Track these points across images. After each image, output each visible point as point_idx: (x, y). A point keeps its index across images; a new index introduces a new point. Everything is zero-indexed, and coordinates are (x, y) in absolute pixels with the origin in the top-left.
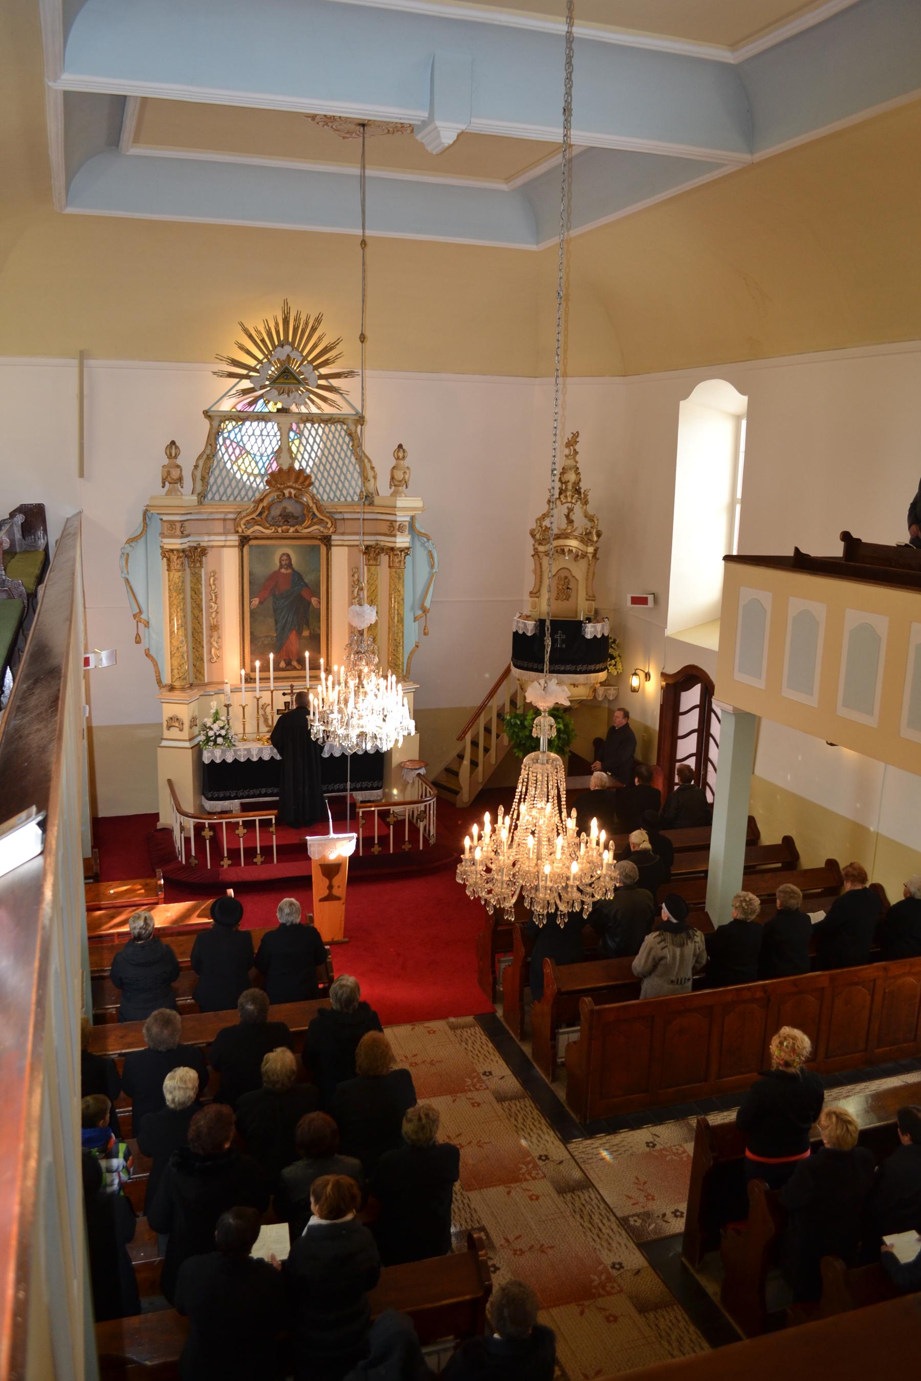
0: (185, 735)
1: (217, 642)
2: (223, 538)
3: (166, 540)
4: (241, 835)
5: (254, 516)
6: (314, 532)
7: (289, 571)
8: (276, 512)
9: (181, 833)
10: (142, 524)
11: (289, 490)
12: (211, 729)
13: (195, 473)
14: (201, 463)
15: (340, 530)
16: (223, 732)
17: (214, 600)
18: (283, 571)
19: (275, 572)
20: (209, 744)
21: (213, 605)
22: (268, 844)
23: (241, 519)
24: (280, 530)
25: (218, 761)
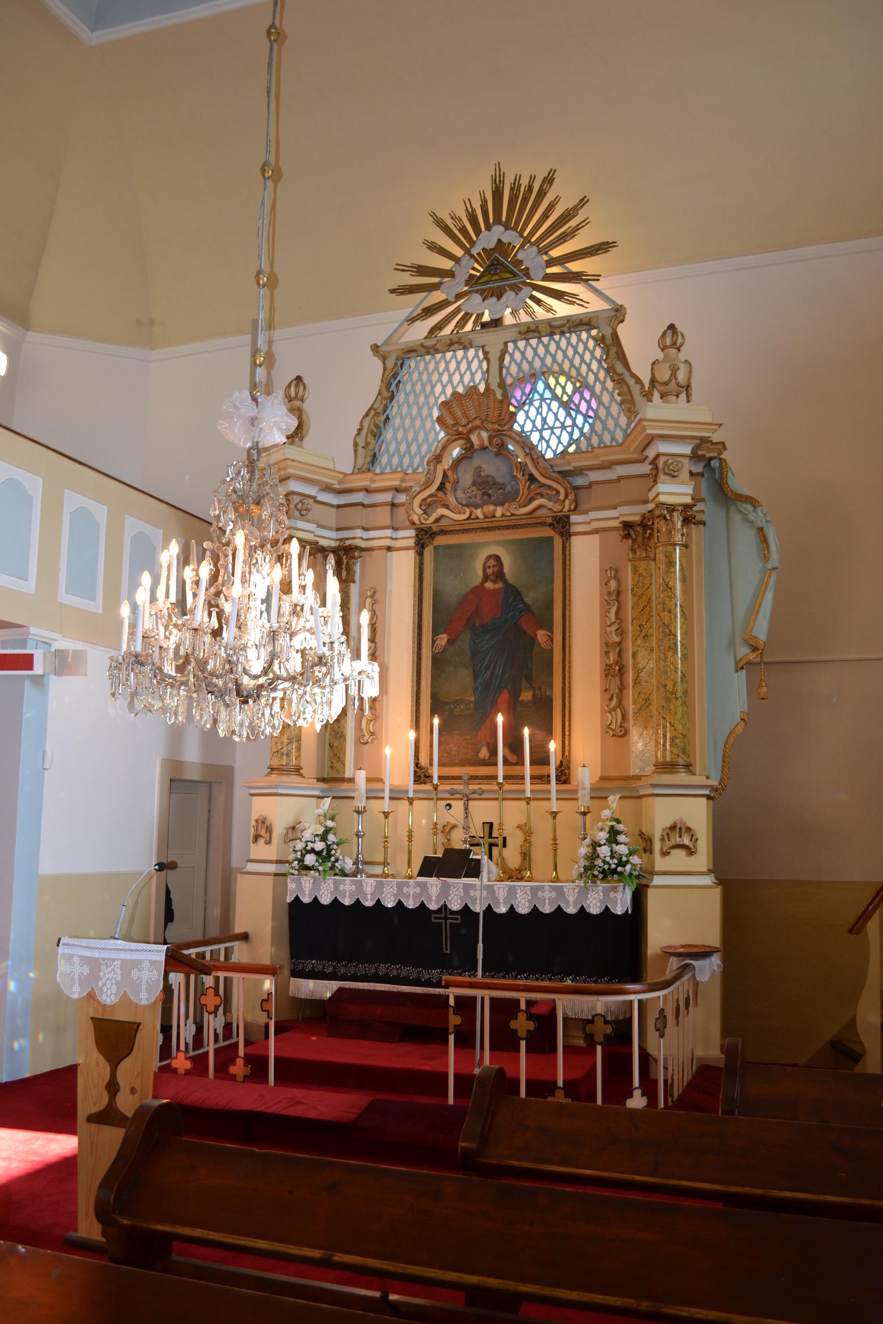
2: (388, 533)
7: (499, 585)
13: (358, 440)
18: (489, 585)
19: (476, 588)
24: (479, 513)
25: (306, 900)
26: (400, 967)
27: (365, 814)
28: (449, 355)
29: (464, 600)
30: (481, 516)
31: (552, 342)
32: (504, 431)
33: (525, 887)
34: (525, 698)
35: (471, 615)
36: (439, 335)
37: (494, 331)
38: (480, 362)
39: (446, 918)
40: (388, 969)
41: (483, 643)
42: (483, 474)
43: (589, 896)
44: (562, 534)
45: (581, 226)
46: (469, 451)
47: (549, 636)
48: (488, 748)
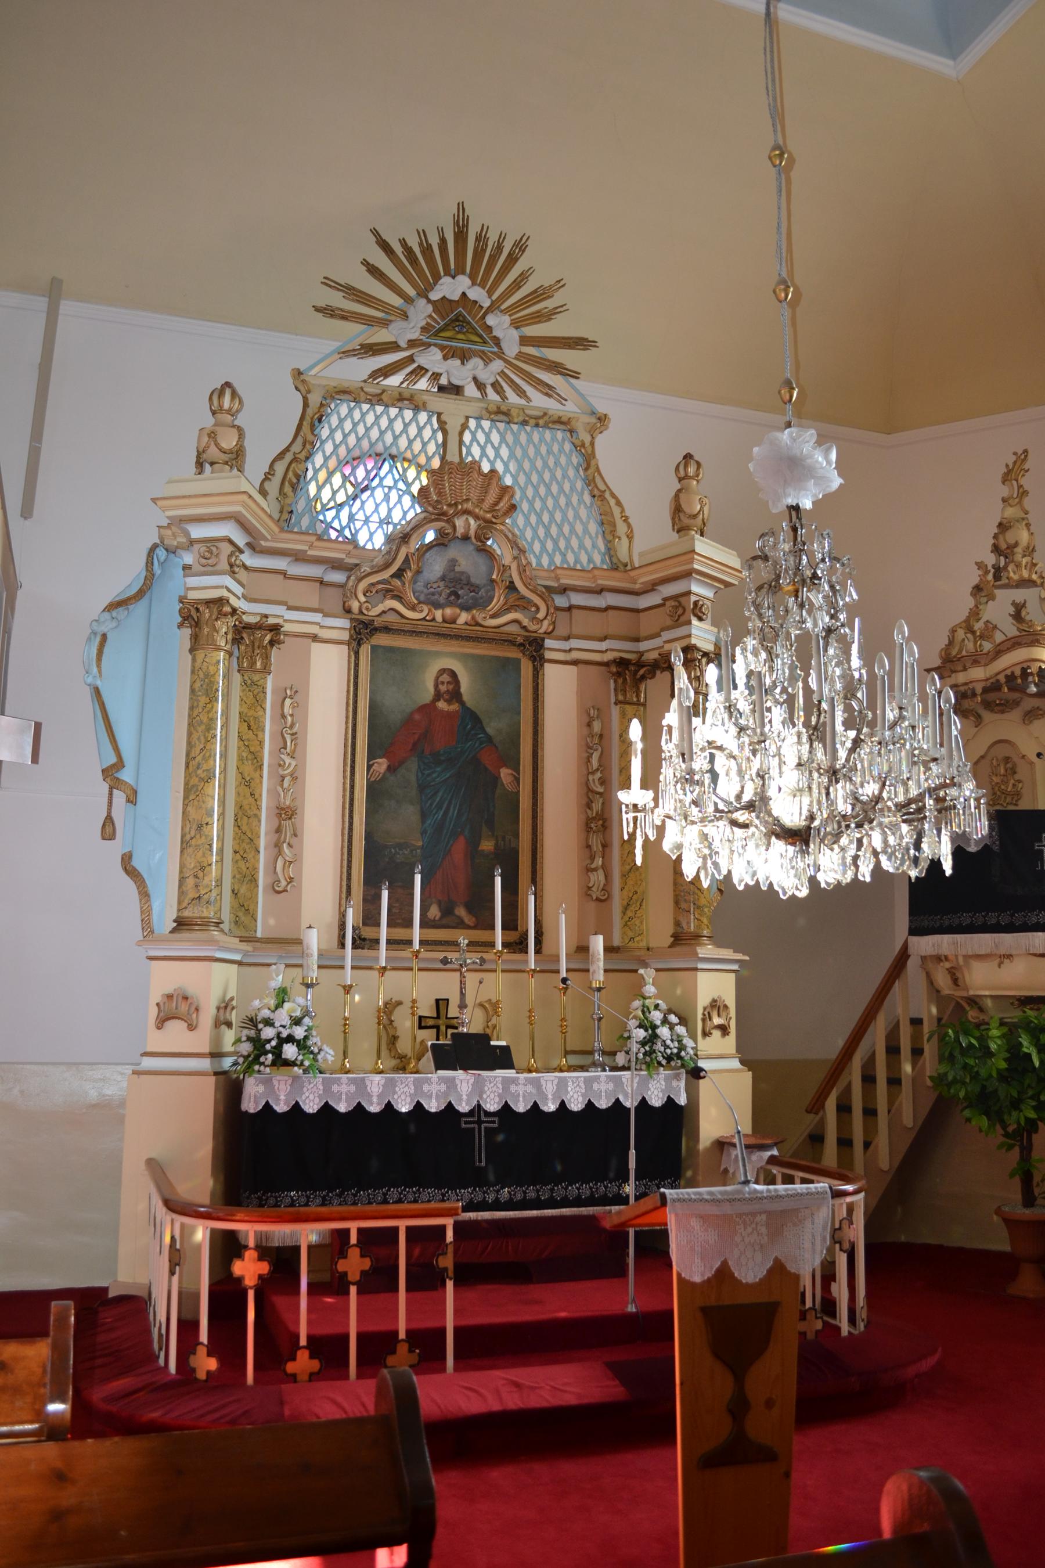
0: (200, 1040)
1: (290, 845)
2: (317, 617)
3: (193, 581)
4: (354, 1276)
5: (386, 575)
6: (506, 629)
7: (455, 707)
8: (435, 567)
9: (172, 1273)
10: (144, 573)
11: (464, 517)
12: (269, 1023)
14: (280, 468)
15: (561, 631)
16: (299, 1032)
17: (288, 750)
18: (442, 705)
19: (424, 709)
20: (262, 1059)
21: (288, 760)
22: (431, 1324)
23: (360, 580)
24: (438, 614)
26: (419, 1190)
27: (316, 987)
28: (393, 411)
29: (408, 722)
30: (439, 618)
31: (372, 413)
32: (496, 524)
33: (577, 1078)
34: (485, 848)
35: (419, 739)
36: (381, 383)
37: (455, 400)
38: (434, 432)
39: (479, 1122)
40: (400, 1194)
41: (434, 775)
42: (457, 569)
43: (650, 1085)
44: (533, 659)
45: (559, 310)
46: (443, 540)
47: (514, 776)
48: (440, 906)
